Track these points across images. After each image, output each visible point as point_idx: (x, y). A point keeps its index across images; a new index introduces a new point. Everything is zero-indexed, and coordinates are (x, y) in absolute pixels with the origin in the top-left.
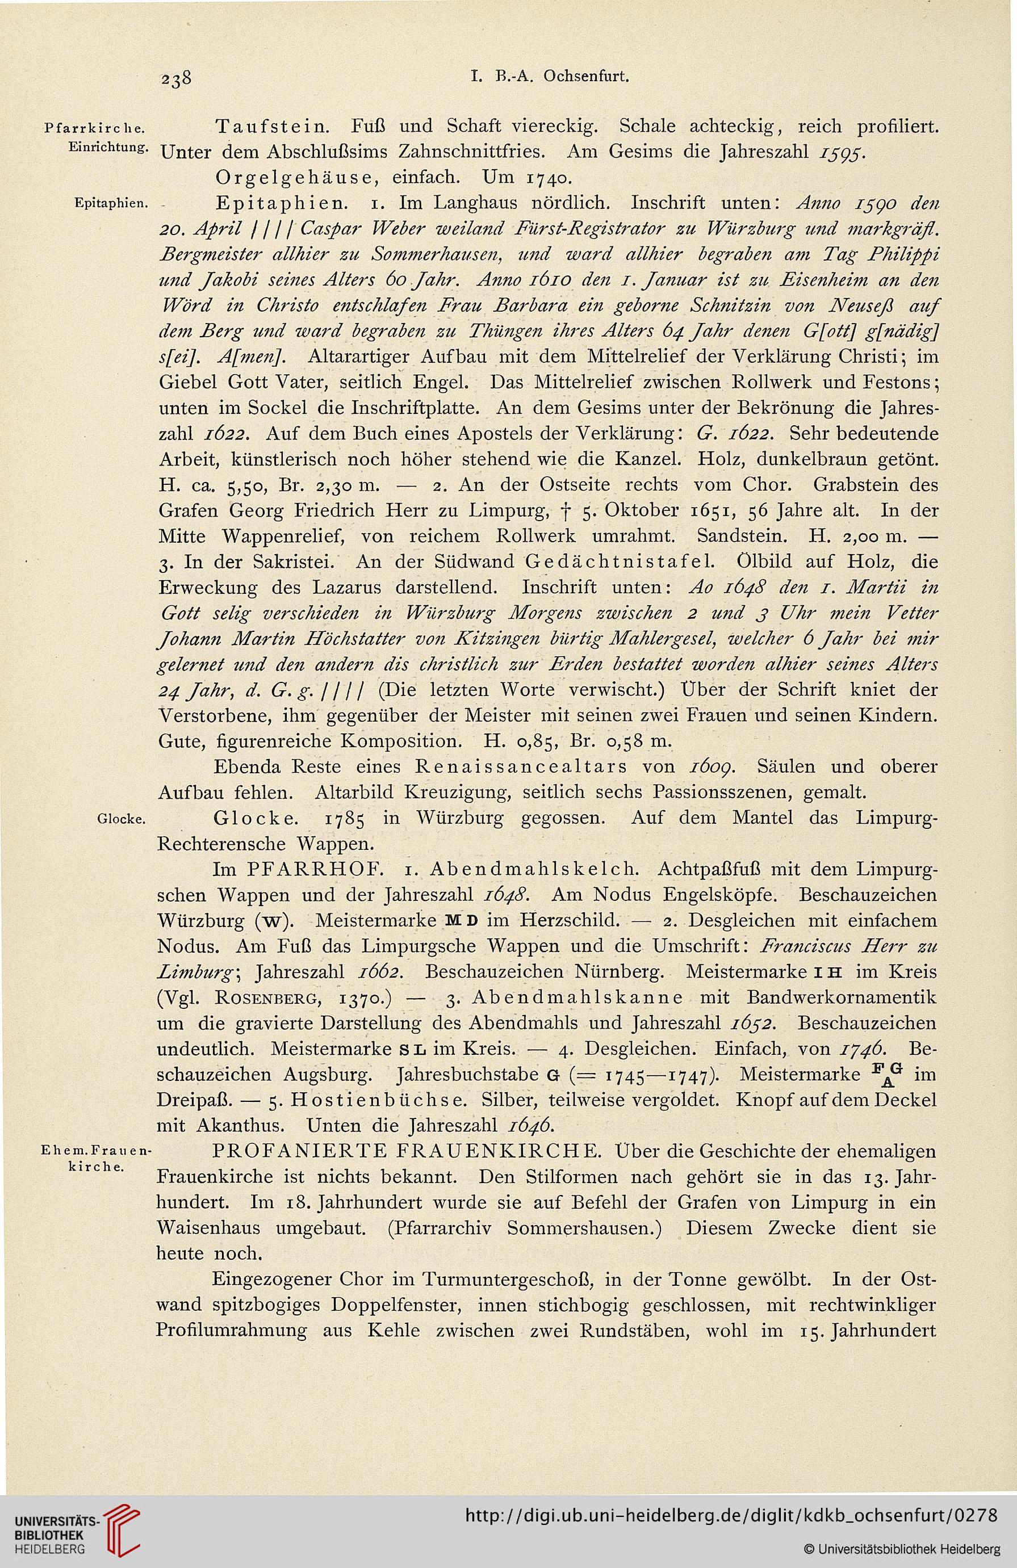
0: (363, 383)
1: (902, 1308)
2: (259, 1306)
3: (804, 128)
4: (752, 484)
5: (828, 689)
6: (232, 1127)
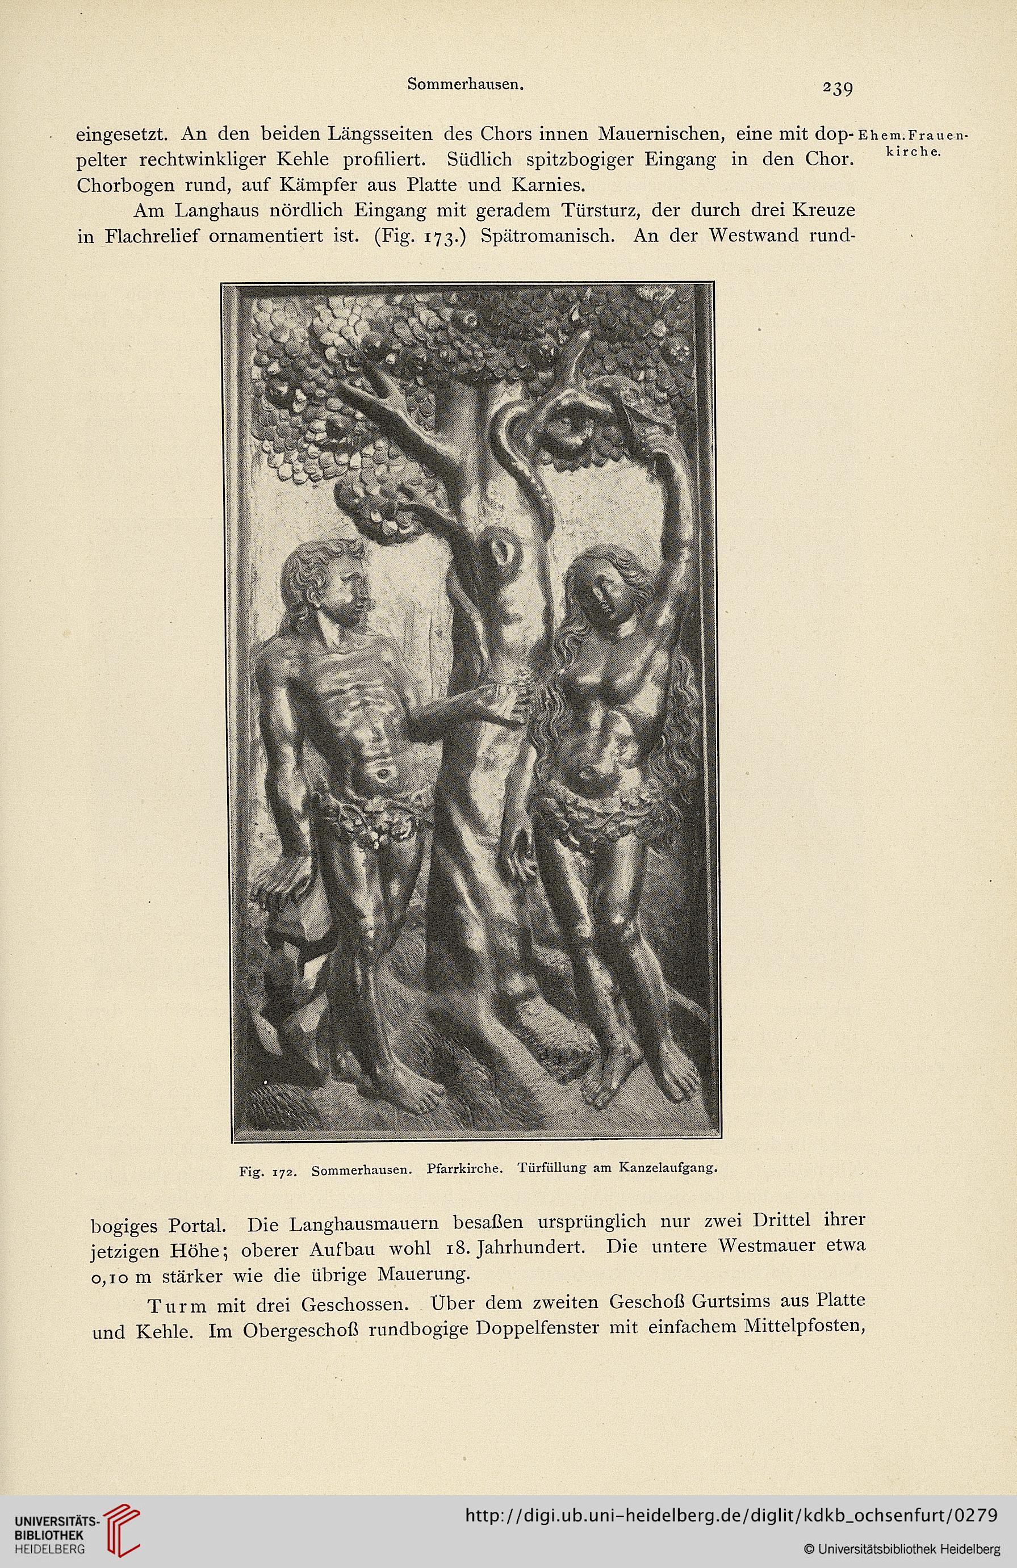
0: (405, 135)
1: (233, 162)
2: (574, 161)
3: (146, 161)
4: (814, 158)
5: (348, 162)
6: (695, 161)
